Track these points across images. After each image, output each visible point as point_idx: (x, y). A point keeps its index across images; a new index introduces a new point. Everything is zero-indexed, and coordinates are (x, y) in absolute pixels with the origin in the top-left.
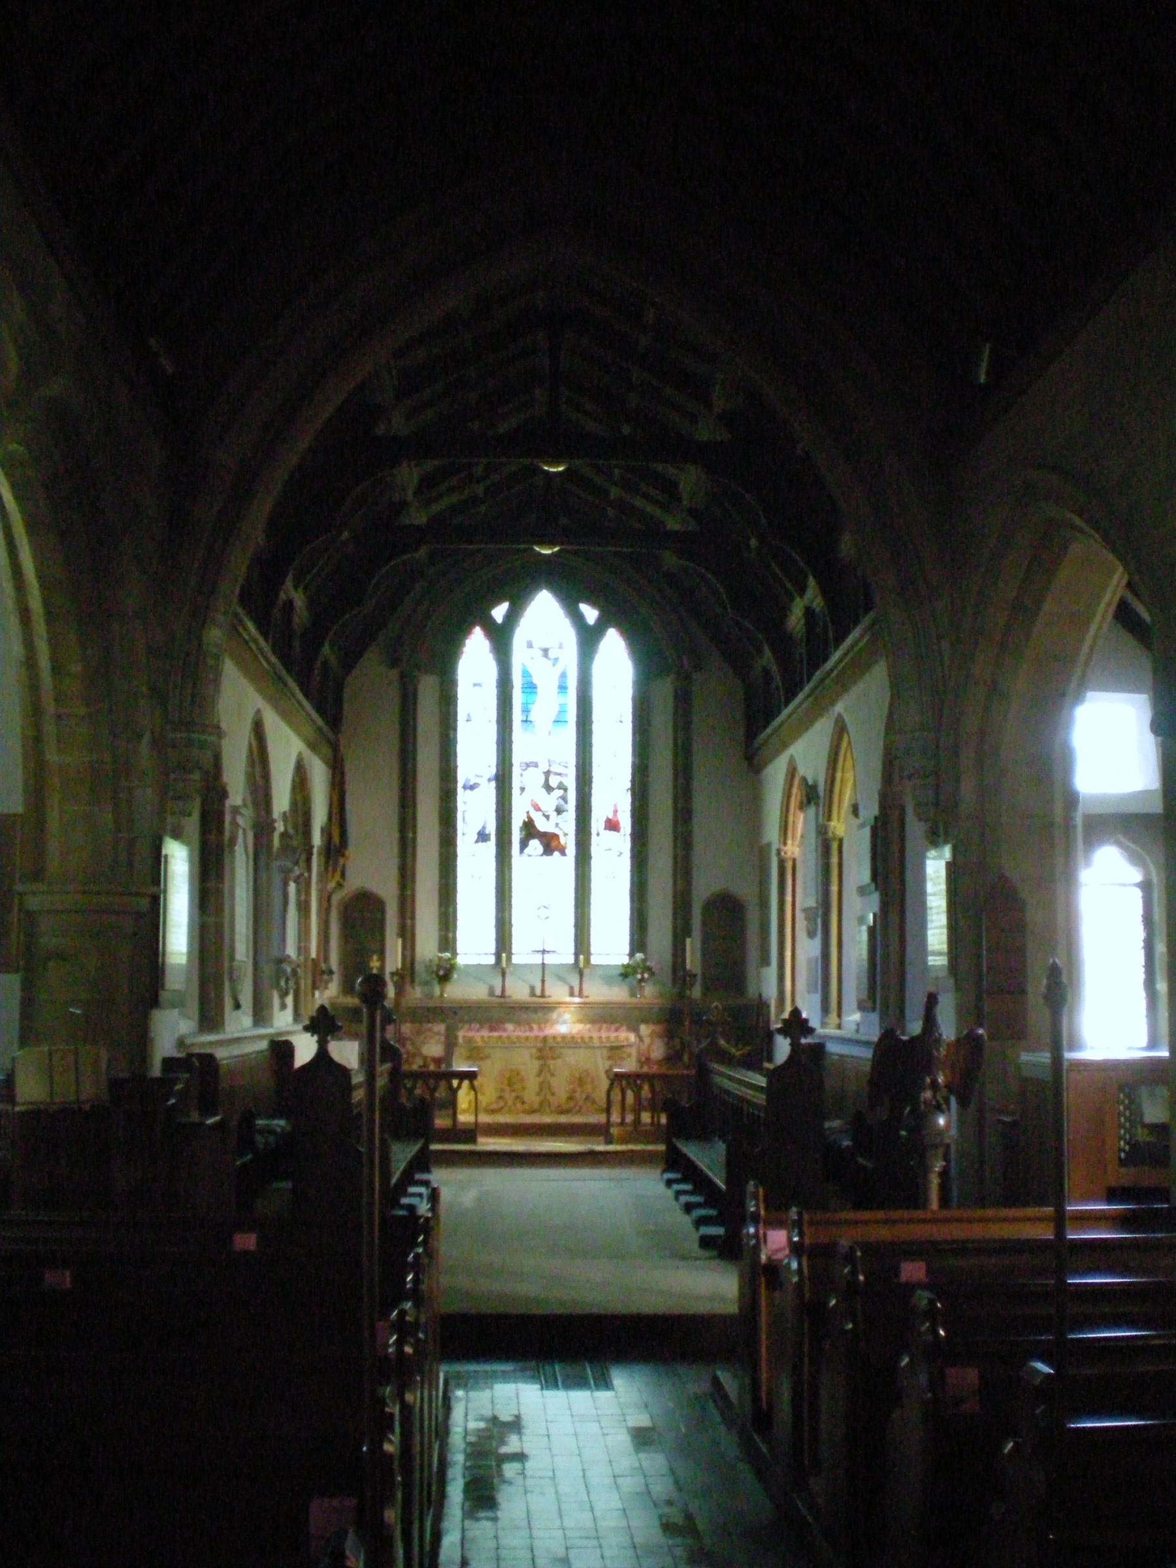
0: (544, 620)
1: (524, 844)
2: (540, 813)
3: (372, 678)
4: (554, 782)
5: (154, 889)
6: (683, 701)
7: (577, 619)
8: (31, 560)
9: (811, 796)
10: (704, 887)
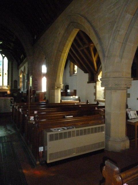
5: (104, 114)
6: (12, 64)
7: (2, 56)
8: (101, 149)
9: (22, 72)
10: (14, 80)
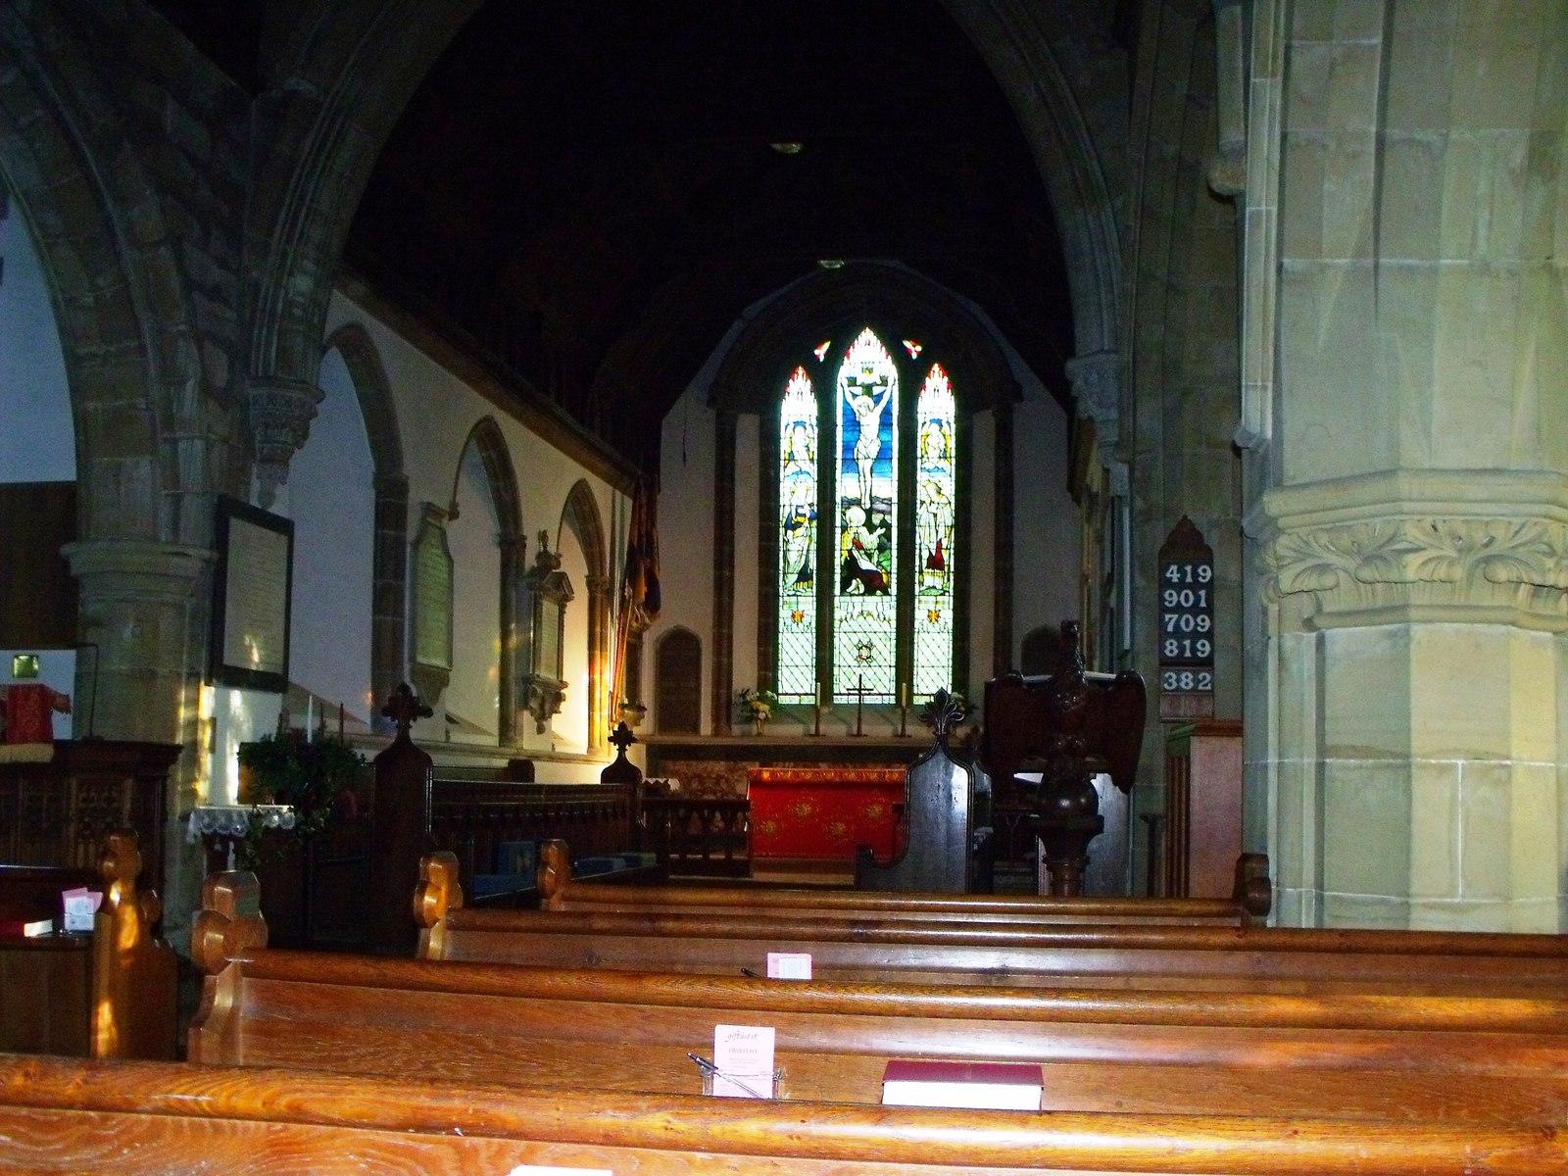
0: (868, 357)
1: (845, 584)
2: (862, 552)
3: (687, 426)
4: (876, 519)
